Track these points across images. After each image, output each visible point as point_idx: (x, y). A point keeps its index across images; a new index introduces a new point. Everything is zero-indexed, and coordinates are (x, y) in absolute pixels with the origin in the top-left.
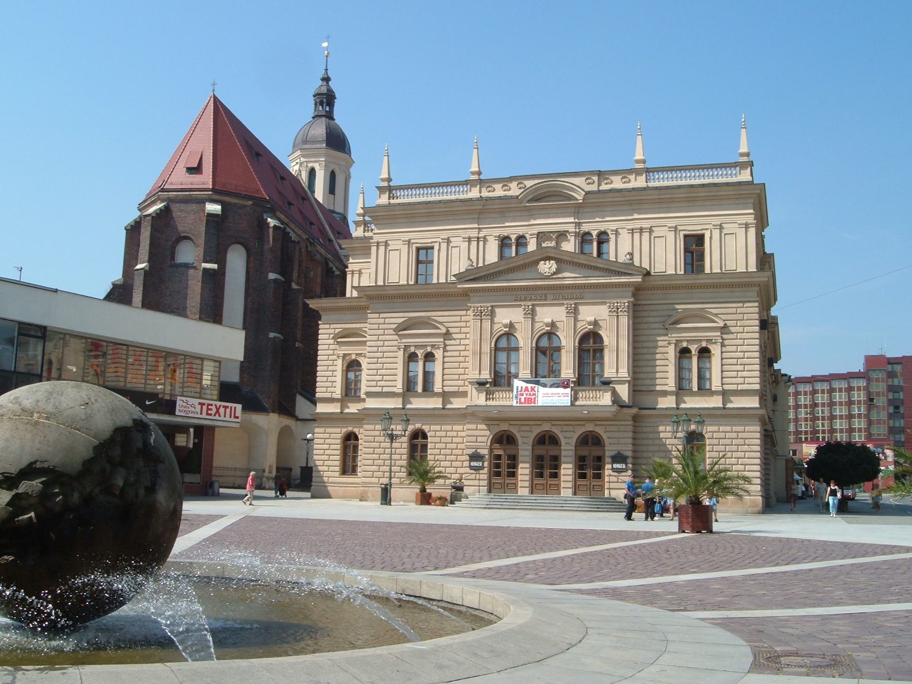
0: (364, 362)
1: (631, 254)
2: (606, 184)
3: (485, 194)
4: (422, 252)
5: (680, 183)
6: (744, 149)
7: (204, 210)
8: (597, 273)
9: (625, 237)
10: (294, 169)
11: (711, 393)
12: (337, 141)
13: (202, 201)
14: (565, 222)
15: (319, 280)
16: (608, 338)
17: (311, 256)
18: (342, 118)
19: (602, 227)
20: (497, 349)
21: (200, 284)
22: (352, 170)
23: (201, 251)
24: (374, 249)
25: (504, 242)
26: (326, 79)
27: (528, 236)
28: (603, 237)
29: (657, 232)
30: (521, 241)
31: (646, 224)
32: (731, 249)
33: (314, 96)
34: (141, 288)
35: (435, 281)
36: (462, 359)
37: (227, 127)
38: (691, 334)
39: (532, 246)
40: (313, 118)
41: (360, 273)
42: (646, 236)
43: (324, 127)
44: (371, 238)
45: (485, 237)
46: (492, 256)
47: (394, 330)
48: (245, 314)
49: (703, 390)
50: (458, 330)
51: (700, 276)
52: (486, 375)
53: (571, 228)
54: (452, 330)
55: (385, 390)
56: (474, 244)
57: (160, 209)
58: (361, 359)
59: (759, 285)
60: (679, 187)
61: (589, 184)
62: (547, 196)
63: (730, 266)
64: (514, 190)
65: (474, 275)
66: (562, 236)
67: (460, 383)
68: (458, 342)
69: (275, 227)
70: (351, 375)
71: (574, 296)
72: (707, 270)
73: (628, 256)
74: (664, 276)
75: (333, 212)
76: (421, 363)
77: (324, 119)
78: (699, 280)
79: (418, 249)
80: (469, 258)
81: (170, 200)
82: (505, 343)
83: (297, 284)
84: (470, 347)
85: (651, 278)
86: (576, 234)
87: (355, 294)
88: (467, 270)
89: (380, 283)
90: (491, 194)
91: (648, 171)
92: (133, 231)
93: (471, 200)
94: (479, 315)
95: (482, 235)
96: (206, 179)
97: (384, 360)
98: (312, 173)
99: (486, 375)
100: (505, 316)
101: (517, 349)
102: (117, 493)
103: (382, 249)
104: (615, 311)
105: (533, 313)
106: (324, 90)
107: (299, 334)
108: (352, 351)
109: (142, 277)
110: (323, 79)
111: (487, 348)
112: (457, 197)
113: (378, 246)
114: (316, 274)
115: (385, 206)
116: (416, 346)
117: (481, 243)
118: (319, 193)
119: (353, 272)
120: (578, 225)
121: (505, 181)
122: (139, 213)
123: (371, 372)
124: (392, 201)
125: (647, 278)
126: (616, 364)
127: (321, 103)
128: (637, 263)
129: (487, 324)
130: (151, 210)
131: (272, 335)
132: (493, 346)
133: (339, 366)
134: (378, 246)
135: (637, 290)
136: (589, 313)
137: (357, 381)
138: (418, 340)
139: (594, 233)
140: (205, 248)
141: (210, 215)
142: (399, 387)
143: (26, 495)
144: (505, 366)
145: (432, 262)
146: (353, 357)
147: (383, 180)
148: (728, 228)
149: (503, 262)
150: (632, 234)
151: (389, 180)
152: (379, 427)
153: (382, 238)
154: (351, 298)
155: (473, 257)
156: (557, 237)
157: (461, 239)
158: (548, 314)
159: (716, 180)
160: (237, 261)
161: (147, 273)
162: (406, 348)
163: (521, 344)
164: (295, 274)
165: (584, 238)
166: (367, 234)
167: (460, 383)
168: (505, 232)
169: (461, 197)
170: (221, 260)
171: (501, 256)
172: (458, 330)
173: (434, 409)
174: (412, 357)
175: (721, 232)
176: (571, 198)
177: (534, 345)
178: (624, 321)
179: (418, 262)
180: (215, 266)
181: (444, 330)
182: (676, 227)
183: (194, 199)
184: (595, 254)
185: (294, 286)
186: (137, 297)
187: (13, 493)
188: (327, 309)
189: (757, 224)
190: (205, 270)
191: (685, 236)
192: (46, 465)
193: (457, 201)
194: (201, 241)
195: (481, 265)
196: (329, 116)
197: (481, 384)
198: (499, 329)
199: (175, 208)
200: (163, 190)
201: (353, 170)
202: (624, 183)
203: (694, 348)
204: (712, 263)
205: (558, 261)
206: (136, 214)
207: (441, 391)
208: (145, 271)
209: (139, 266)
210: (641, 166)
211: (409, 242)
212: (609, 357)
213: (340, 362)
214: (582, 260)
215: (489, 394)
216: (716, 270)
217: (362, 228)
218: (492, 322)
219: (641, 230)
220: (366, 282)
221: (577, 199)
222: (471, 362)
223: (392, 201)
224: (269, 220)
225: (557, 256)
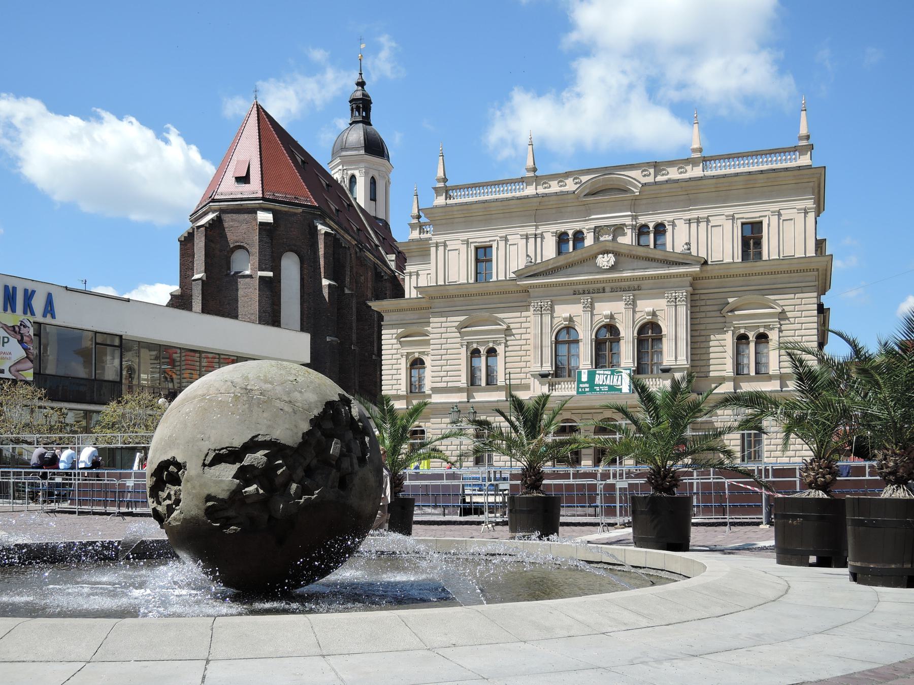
0: (428, 360)
1: (688, 244)
2: (663, 175)
3: (541, 190)
4: (481, 251)
5: (738, 170)
6: (803, 131)
7: (256, 219)
8: (654, 264)
9: (681, 226)
10: (337, 176)
11: (770, 378)
12: (374, 147)
13: (253, 211)
14: (623, 217)
15: (370, 285)
16: (666, 328)
17: (362, 261)
18: (380, 123)
19: (659, 218)
20: (557, 342)
21: (257, 291)
22: (391, 176)
23: (255, 259)
24: (433, 250)
25: (562, 238)
26: (361, 84)
27: (585, 231)
28: (660, 229)
29: (714, 221)
30: (579, 236)
31: (703, 214)
32: (789, 233)
33: (350, 102)
34: (200, 298)
35: (494, 278)
36: (523, 353)
37: (275, 137)
38: (749, 318)
39: (589, 241)
40: (351, 124)
41: (418, 275)
42: (703, 225)
43: (362, 133)
44: (430, 239)
45: (542, 234)
46: (549, 250)
47: (456, 327)
48: (301, 319)
49: (761, 373)
50: (518, 325)
51: (758, 264)
52: (548, 368)
53: (628, 221)
54: (512, 326)
55: (450, 385)
56: (532, 241)
57: (212, 219)
58: (424, 358)
59: (818, 270)
60: (737, 175)
61: (645, 176)
62: (605, 187)
63: (788, 252)
64: (570, 185)
65: (533, 271)
66: (618, 230)
67: (523, 376)
68: (518, 337)
69: (326, 233)
70: (415, 372)
71: (633, 290)
72: (765, 257)
73: (686, 247)
74: (720, 264)
75: (376, 218)
76: (483, 358)
77: (361, 125)
78: (756, 266)
79: (477, 248)
80: (528, 256)
81: (223, 211)
82: (565, 337)
83: (349, 289)
84: (531, 342)
85: (709, 268)
86: (633, 227)
87: (414, 294)
88: (526, 267)
89: (441, 282)
90: (547, 191)
91: (705, 160)
92: (187, 242)
93: (527, 197)
94: (540, 311)
95: (539, 232)
96: (254, 187)
97: (448, 357)
98: (353, 179)
99: (548, 368)
100: (563, 311)
101: (577, 341)
102: (334, 463)
103: (441, 249)
104: (674, 302)
105: (592, 308)
106: (359, 95)
107: (354, 337)
108: (416, 351)
109: (200, 287)
110: (358, 84)
111: (548, 340)
112: (514, 194)
113: (437, 247)
114: (367, 279)
115: (442, 207)
116: (478, 343)
117: (539, 240)
118: (360, 196)
119: (410, 274)
120: (635, 218)
121: (561, 177)
122: (191, 224)
123: (435, 369)
124: (449, 202)
125: (705, 268)
126: (674, 352)
127: (358, 109)
128: (694, 253)
129: (547, 319)
130: (203, 221)
131: (328, 339)
132: (553, 339)
133: (403, 364)
134: (437, 247)
135: (695, 278)
136: (646, 307)
137: (421, 379)
138: (482, 335)
139: (651, 225)
140: (260, 255)
141: (262, 225)
142: (463, 381)
143: (251, 467)
144: (566, 358)
145: (491, 260)
146: (417, 355)
147: (439, 180)
148: (785, 214)
149: (562, 257)
150: (690, 223)
151: (445, 180)
152: (448, 420)
153: (440, 239)
154: (410, 299)
155: (532, 254)
156: (614, 231)
157: (519, 236)
158: (604, 309)
159: (774, 166)
160: (290, 267)
161: (204, 283)
162: (408, 354)
163: (581, 336)
164: (348, 280)
165: (642, 231)
166: (422, 236)
167: (523, 376)
168: (562, 228)
169: (518, 194)
170: (277, 269)
171: (559, 252)
172: (518, 325)
173: (498, 401)
174: (475, 353)
175: (779, 219)
176: (626, 191)
177: (593, 337)
178: (683, 311)
179: (477, 261)
180: (271, 274)
181: (505, 327)
182: (733, 216)
183: (245, 209)
184: (652, 246)
185: (347, 291)
186: (197, 304)
187: (238, 465)
188: (387, 311)
189: (815, 208)
190: (261, 278)
191: (743, 224)
192: (268, 438)
193: (512, 199)
194: (255, 250)
195: (539, 261)
196: (366, 121)
197: (544, 376)
198: (559, 322)
199: (226, 218)
200: (214, 201)
201: (392, 176)
202: (681, 173)
203: (752, 336)
204: (770, 249)
205: (616, 254)
206: (188, 226)
207: (504, 384)
208: (203, 281)
209: (196, 276)
210: (698, 155)
211: (467, 242)
212: (667, 346)
213: (403, 360)
214: (641, 251)
215: (552, 386)
216: (774, 256)
217: (418, 231)
218: (552, 317)
219: (698, 221)
220: (423, 282)
221: (634, 192)
222: (532, 356)
223: (449, 202)
224: (320, 227)
225: (615, 250)
